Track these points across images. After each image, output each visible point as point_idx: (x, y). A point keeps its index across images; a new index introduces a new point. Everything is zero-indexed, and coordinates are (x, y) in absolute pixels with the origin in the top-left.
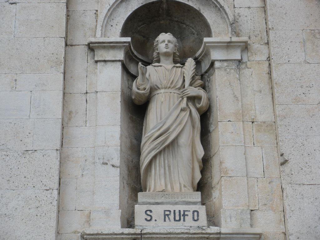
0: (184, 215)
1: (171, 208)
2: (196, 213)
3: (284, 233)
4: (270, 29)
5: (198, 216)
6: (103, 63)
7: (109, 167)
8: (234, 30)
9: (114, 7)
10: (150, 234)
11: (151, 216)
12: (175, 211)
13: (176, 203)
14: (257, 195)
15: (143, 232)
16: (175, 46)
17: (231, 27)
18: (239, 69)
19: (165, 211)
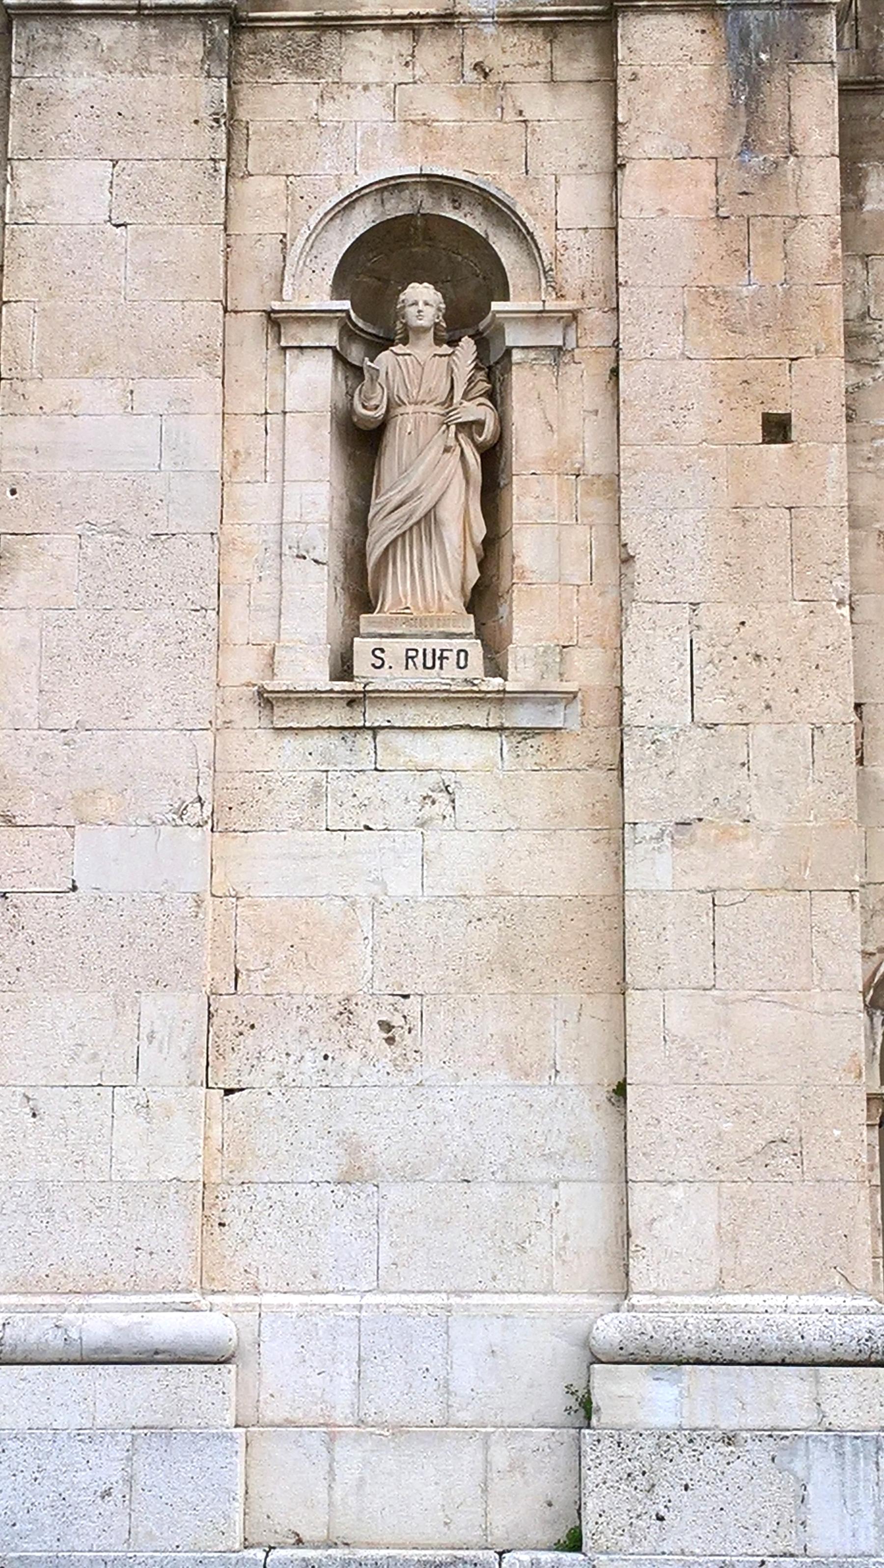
0: (441, 658)
1: (419, 644)
2: (462, 654)
3: (618, 687)
4: (621, 284)
5: (466, 659)
6: (296, 351)
7: (309, 563)
8: (553, 284)
9: (317, 232)
10: (380, 691)
11: (382, 659)
12: (425, 650)
13: (428, 636)
14: (575, 619)
15: (368, 688)
16: (439, 309)
17: (546, 278)
18: (558, 365)
19: (408, 650)
